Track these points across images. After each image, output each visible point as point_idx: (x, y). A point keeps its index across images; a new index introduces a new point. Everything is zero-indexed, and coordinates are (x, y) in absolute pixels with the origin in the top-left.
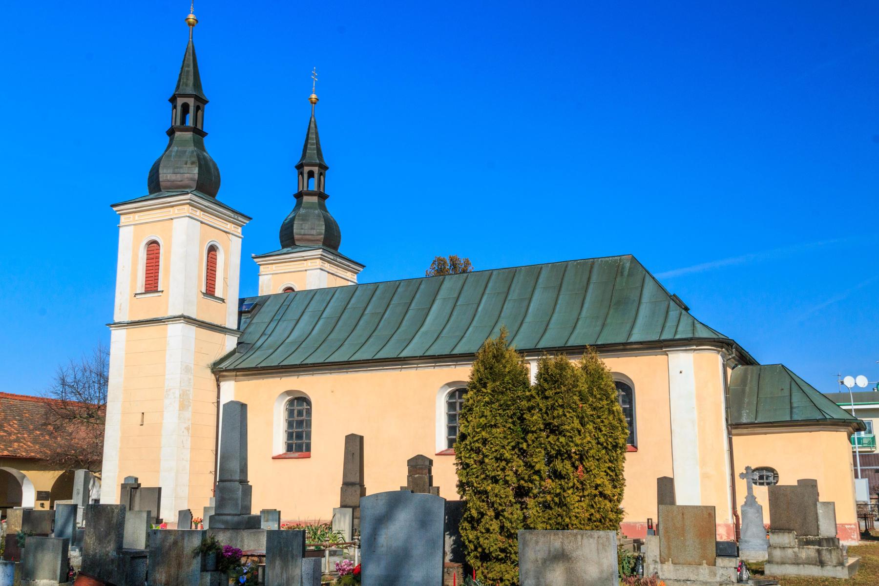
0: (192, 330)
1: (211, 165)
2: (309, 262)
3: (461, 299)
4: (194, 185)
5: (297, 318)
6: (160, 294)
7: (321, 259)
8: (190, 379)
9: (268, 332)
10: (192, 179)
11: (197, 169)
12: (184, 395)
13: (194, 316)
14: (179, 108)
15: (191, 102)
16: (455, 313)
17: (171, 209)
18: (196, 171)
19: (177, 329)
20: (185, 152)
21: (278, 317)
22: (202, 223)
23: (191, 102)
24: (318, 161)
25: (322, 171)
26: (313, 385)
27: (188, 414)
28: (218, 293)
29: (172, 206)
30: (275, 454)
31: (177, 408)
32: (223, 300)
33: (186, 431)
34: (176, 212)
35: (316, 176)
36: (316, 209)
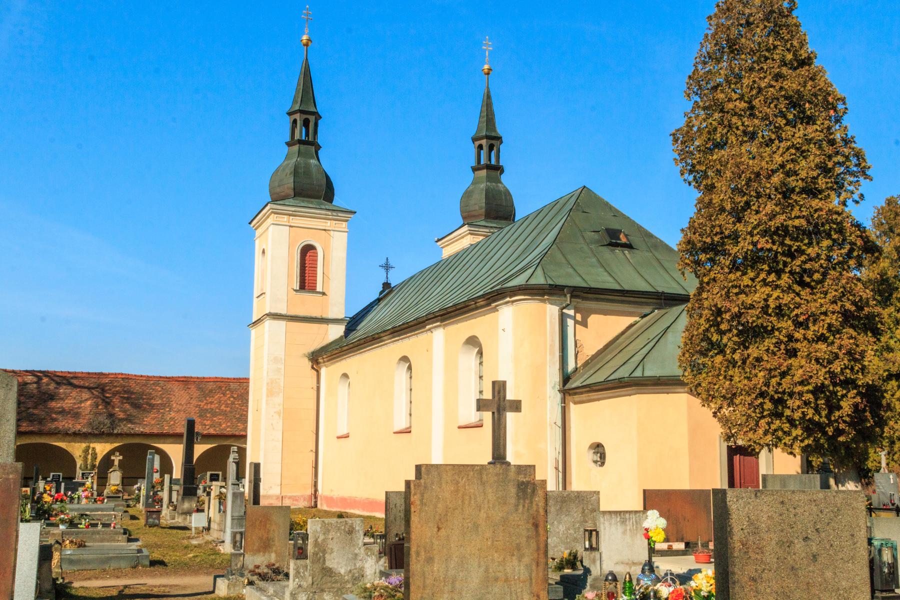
13: (284, 312)
19: (268, 323)
22: (290, 226)
28: (319, 288)
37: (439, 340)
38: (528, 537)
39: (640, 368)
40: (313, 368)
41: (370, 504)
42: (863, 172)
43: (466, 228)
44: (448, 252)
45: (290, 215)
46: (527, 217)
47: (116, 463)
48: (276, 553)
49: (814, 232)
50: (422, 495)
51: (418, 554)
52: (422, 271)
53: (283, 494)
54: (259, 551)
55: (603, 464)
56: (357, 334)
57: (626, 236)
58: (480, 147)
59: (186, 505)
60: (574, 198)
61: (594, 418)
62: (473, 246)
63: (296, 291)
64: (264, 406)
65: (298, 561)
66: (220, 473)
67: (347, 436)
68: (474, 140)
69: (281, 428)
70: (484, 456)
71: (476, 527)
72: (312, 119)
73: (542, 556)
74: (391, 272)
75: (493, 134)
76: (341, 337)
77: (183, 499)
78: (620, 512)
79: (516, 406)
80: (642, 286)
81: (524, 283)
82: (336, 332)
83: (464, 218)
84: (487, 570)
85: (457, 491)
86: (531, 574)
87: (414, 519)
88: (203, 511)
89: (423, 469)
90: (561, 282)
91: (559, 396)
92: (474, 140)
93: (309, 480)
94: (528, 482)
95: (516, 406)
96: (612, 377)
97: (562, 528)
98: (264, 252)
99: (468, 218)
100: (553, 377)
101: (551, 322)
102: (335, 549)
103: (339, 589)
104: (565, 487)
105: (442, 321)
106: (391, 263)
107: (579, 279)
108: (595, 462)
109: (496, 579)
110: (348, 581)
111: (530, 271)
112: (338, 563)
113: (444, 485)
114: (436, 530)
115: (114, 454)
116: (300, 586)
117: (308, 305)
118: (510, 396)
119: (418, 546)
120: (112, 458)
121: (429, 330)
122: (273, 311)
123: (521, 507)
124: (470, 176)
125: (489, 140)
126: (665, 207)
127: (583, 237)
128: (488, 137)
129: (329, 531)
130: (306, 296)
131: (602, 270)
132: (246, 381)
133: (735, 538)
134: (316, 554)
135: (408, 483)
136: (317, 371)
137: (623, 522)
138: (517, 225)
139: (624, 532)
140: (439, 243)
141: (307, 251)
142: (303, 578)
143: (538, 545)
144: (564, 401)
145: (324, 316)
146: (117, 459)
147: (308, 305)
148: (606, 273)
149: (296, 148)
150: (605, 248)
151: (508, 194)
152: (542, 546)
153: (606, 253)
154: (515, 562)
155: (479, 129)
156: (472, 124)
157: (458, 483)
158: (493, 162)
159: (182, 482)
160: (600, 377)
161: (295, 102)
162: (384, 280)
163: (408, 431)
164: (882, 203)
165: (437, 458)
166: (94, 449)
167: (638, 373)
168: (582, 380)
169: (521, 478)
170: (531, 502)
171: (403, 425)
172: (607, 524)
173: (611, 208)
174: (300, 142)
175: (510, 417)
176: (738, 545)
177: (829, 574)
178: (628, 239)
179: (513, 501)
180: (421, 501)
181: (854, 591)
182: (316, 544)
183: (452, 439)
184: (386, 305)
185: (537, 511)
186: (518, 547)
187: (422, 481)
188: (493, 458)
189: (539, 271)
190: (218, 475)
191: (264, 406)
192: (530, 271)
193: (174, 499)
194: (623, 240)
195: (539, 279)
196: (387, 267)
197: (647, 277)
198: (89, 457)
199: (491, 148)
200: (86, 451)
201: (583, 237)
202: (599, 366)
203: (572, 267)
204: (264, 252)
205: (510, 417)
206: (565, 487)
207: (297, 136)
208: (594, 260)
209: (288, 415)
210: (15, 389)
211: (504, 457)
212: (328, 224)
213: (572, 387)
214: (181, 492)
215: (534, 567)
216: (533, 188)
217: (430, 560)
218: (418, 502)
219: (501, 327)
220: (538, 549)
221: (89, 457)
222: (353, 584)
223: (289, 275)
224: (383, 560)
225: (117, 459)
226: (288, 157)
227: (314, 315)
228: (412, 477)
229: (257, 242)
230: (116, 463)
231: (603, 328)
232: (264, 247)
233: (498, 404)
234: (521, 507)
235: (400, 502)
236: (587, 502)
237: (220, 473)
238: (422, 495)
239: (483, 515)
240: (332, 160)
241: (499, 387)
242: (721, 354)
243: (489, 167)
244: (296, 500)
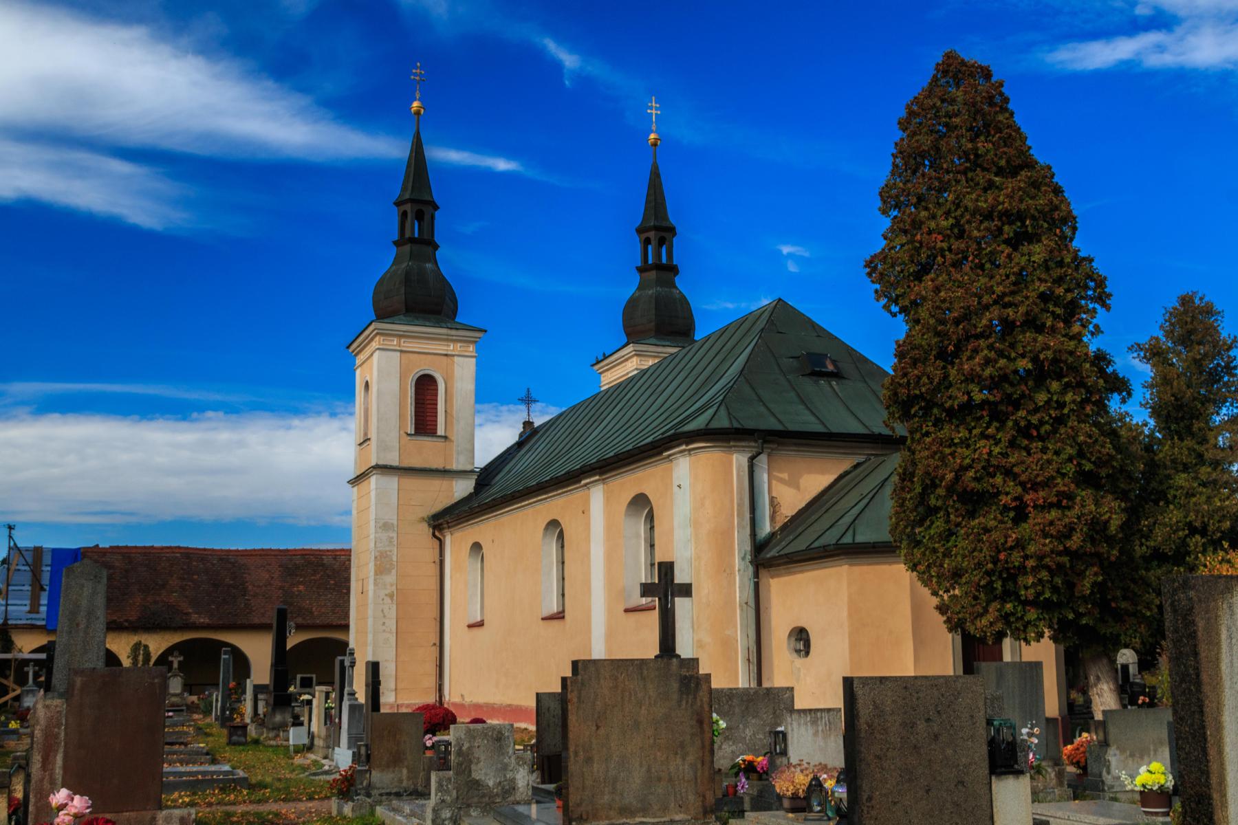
0: (392, 482)
13: (396, 463)
22: (401, 351)
27: (390, 579)
28: (441, 431)
32: (445, 437)
33: (388, 600)
37: (597, 507)
38: (692, 735)
39: (850, 532)
40: (434, 535)
41: (516, 711)
42: (1102, 299)
43: (630, 348)
44: (610, 378)
45: (400, 336)
46: (709, 337)
47: (176, 665)
48: (407, 767)
49: (1040, 375)
50: (580, 692)
51: (576, 753)
52: (574, 407)
53: (400, 702)
54: (388, 767)
55: (807, 653)
56: (495, 490)
57: (834, 362)
58: (647, 242)
59: (278, 718)
60: (766, 315)
61: (800, 596)
62: (643, 373)
64: (371, 587)
65: (441, 773)
66: (314, 676)
67: (480, 624)
68: (640, 231)
70: (649, 648)
71: (637, 724)
72: (427, 210)
73: (707, 753)
75: (664, 224)
77: (274, 710)
78: (810, 710)
79: (686, 590)
80: (855, 428)
81: (703, 426)
82: (463, 488)
83: (628, 334)
84: (649, 770)
85: (616, 687)
86: (696, 773)
87: (572, 719)
88: (301, 724)
89: (855, 682)
90: (750, 424)
91: (751, 569)
93: (431, 682)
94: (692, 676)
95: (686, 590)
96: (816, 544)
97: (748, 732)
98: (367, 385)
99: (634, 334)
100: (740, 545)
101: (738, 475)
102: (482, 758)
103: (487, 804)
104: (760, 682)
105: (601, 474)
107: (772, 420)
108: (798, 651)
109: (659, 779)
110: (497, 795)
111: (711, 412)
112: (486, 774)
113: (602, 681)
114: (594, 728)
115: (172, 655)
116: (443, 801)
117: (426, 452)
118: (680, 578)
119: (577, 746)
120: (170, 659)
121: (585, 485)
122: (381, 463)
123: (684, 703)
124: (636, 278)
125: (658, 230)
126: (873, 333)
127: (778, 365)
129: (474, 738)
130: (426, 442)
131: (802, 407)
132: (348, 553)
133: (862, 721)
134: (459, 764)
135: (564, 680)
136: (440, 540)
137: (814, 722)
138: (697, 346)
139: (816, 734)
140: (596, 367)
141: (425, 387)
142: (447, 792)
143: (703, 743)
144: (756, 575)
145: (448, 467)
146: (176, 661)
147: (426, 452)
148: (807, 412)
149: (407, 248)
150: (807, 379)
151: (684, 302)
152: (707, 743)
153: (808, 385)
154: (679, 761)
156: (637, 213)
157: (616, 679)
158: (664, 260)
159: (271, 688)
160: (801, 545)
161: (404, 189)
163: (560, 616)
164: (1173, 303)
165: (598, 651)
166: (146, 647)
167: (847, 539)
168: (778, 548)
169: (684, 672)
170: (695, 698)
171: (554, 608)
172: (795, 724)
173: (813, 325)
174: (412, 240)
175: (680, 603)
176: (864, 727)
177: (949, 752)
178: (836, 366)
179: (675, 696)
180: (579, 698)
181: (974, 767)
182: (460, 753)
183: (610, 629)
184: (528, 451)
185: (702, 706)
186: (682, 745)
187: (580, 677)
188: (661, 650)
189: (723, 411)
190: (311, 679)
191: (371, 587)
192: (711, 412)
193: (261, 710)
194: (830, 368)
195: (723, 422)
197: (861, 415)
198: (141, 658)
199: (662, 242)
200: (136, 647)
201: (778, 365)
202: (800, 530)
203: (764, 404)
204: (367, 385)
205: (680, 603)
206: (760, 682)
207: (408, 235)
208: (792, 394)
209: (401, 598)
210: (105, 580)
211: (674, 649)
212: (451, 348)
213: (771, 554)
214: (271, 701)
215: (699, 766)
216: (717, 306)
217: (589, 760)
218: (575, 700)
219: (676, 483)
220: (703, 747)
221: (141, 658)
222: (504, 798)
223: (402, 416)
224: (535, 775)
225: (176, 661)
226: (397, 261)
227: (434, 466)
228: (569, 674)
229: (358, 372)
230: (176, 665)
231: (798, 484)
232: (368, 378)
233: (665, 588)
234: (684, 703)
235: (555, 706)
236: (780, 701)
237: (314, 676)
238: (580, 692)
239: (643, 711)
240: (452, 260)
241: (666, 569)
242: (926, 524)
243: (659, 267)
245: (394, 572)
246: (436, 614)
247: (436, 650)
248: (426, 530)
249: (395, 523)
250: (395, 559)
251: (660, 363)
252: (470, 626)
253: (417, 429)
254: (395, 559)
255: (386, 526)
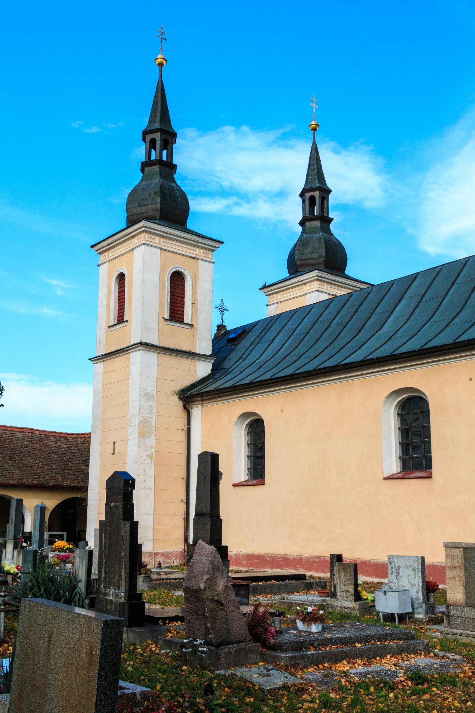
0: (152, 358)
1: (178, 193)
2: (308, 285)
3: (427, 295)
4: (157, 214)
5: (272, 339)
6: (125, 324)
7: (317, 280)
8: (152, 406)
9: (245, 356)
10: (155, 210)
11: (159, 198)
12: (144, 422)
13: (155, 343)
14: (307, 202)
15: (316, 194)
16: (417, 311)
17: (304, 286)
18: (158, 200)
19: (137, 356)
20: (150, 185)
21: (257, 341)
22: (161, 249)
23: (316, 194)
24: (318, 185)
25: (325, 195)
26: (266, 405)
27: (150, 442)
28: (187, 319)
29: (133, 237)
30: (237, 481)
31: (137, 435)
32: (192, 325)
33: (148, 460)
34: (136, 241)
35: (317, 201)
36: (317, 233)
63: (166, 320)
69: (153, 474)
74: (226, 314)
76: (209, 375)
82: (203, 369)
92: (145, 133)
106: (226, 305)
128: (160, 130)
141: (177, 280)
147: (177, 337)
155: (152, 120)
162: (219, 323)
196: (222, 309)
223: (161, 304)
227: (184, 349)
244: (169, 557)
245: (153, 436)
246: (184, 475)
247: (183, 505)
248: (177, 404)
249: (155, 393)
250: (154, 425)
251: (350, 296)
252: (234, 485)
253: (171, 316)
254: (154, 425)
255: (148, 396)
